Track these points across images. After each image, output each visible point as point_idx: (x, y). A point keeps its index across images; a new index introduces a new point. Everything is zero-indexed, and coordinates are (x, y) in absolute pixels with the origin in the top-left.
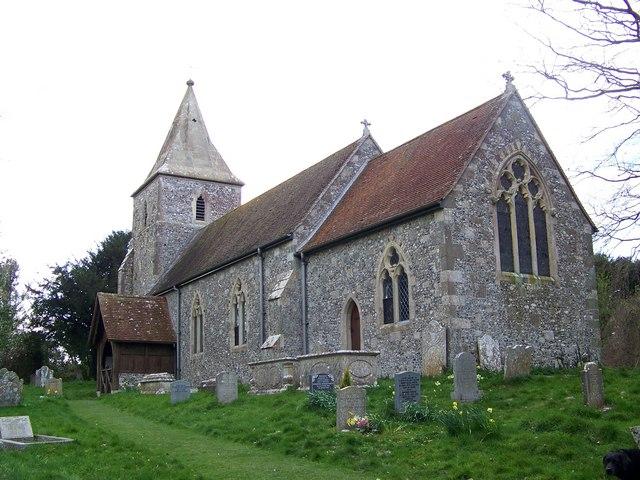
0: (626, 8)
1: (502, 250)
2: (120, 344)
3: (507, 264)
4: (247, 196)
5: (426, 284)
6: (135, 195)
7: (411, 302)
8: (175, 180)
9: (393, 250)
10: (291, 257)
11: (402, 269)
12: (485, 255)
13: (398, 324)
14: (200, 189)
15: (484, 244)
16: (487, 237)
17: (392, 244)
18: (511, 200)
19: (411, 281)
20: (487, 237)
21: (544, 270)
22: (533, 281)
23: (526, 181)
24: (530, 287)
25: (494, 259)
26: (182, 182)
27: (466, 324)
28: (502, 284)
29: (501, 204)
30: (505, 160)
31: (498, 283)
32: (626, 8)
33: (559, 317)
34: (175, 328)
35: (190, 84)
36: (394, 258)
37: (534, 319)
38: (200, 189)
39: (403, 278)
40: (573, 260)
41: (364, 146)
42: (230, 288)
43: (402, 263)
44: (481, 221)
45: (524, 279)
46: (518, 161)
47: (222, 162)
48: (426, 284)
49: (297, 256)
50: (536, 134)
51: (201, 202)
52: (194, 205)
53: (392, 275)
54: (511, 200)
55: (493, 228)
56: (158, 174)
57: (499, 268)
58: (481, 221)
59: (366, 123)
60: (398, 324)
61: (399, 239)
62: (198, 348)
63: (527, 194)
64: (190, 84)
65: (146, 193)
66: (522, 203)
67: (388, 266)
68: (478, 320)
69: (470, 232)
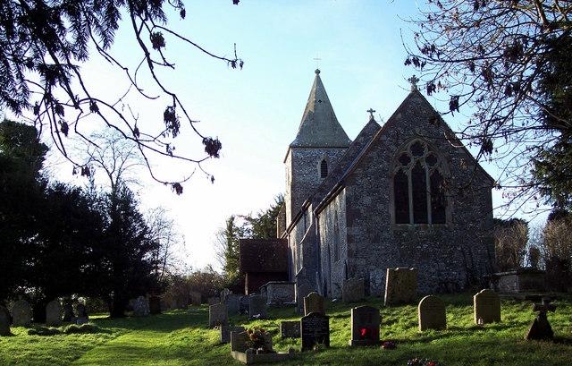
0: (87, 97)
3: (401, 217)
8: (303, 150)
14: (323, 154)
15: (380, 207)
16: (383, 201)
18: (409, 173)
20: (383, 201)
22: (426, 228)
24: (422, 232)
25: (389, 217)
26: (308, 151)
27: (363, 262)
28: (395, 233)
31: (391, 232)
32: (87, 97)
33: (451, 253)
38: (323, 154)
45: (417, 228)
46: (417, 143)
52: (319, 167)
54: (409, 173)
55: (389, 195)
59: (371, 111)
63: (425, 165)
66: (418, 173)
68: (373, 259)
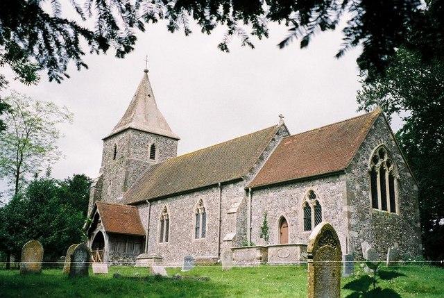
1: (373, 198)
2: (114, 237)
3: (375, 205)
4: (183, 150)
5: (333, 212)
6: (105, 140)
7: (169, 231)
9: (312, 192)
10: (242, 189)
11: (317, 202)
12: (364, 198)
13: (200, 239)
14: (153, 140)
15: (364, 193)
17: (311, 188)
18: (378, 170)
19: (324, 209)
20: (364, 188)
21: (393, 210)
23: (385, 160)
25: (369, 201)
26: (143, 135)
29: (373, 174)
30: (375, 149)
34: (145, 226)
35: (146, 71)
36: (312, 195)
37: (389, 235)
39: (168, 220)
40: (407, 205)
41: (282, 130)
42: (194, 204)
43: (318, 199)
44: (363, 181)
47: (166, 125)
48: (333, 212)
49: (247, 190)
50: (391, 135)
51: (153, 147)
52: (149, 149)
53: (311, 205)
54: (378, 170)
55: (368, 185)
56: (129, 128)
57: (371, 207)
58: (363, 181)
59: (281, 117)
60: (200, 239)
61: (319, 188)
62: (164, 239)
64: (146, 71)
65: (116, 141)
67: (308, 200)
69: (358, 187)
